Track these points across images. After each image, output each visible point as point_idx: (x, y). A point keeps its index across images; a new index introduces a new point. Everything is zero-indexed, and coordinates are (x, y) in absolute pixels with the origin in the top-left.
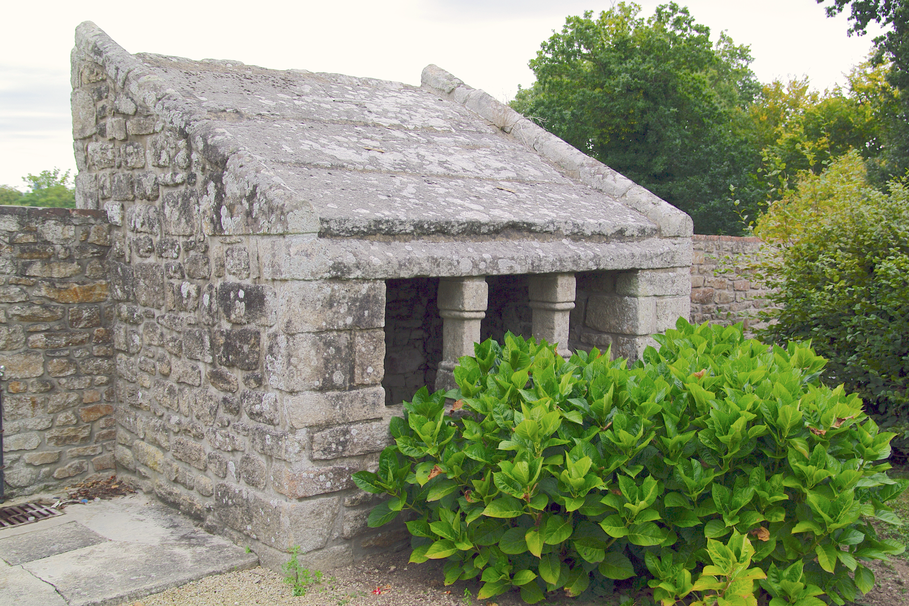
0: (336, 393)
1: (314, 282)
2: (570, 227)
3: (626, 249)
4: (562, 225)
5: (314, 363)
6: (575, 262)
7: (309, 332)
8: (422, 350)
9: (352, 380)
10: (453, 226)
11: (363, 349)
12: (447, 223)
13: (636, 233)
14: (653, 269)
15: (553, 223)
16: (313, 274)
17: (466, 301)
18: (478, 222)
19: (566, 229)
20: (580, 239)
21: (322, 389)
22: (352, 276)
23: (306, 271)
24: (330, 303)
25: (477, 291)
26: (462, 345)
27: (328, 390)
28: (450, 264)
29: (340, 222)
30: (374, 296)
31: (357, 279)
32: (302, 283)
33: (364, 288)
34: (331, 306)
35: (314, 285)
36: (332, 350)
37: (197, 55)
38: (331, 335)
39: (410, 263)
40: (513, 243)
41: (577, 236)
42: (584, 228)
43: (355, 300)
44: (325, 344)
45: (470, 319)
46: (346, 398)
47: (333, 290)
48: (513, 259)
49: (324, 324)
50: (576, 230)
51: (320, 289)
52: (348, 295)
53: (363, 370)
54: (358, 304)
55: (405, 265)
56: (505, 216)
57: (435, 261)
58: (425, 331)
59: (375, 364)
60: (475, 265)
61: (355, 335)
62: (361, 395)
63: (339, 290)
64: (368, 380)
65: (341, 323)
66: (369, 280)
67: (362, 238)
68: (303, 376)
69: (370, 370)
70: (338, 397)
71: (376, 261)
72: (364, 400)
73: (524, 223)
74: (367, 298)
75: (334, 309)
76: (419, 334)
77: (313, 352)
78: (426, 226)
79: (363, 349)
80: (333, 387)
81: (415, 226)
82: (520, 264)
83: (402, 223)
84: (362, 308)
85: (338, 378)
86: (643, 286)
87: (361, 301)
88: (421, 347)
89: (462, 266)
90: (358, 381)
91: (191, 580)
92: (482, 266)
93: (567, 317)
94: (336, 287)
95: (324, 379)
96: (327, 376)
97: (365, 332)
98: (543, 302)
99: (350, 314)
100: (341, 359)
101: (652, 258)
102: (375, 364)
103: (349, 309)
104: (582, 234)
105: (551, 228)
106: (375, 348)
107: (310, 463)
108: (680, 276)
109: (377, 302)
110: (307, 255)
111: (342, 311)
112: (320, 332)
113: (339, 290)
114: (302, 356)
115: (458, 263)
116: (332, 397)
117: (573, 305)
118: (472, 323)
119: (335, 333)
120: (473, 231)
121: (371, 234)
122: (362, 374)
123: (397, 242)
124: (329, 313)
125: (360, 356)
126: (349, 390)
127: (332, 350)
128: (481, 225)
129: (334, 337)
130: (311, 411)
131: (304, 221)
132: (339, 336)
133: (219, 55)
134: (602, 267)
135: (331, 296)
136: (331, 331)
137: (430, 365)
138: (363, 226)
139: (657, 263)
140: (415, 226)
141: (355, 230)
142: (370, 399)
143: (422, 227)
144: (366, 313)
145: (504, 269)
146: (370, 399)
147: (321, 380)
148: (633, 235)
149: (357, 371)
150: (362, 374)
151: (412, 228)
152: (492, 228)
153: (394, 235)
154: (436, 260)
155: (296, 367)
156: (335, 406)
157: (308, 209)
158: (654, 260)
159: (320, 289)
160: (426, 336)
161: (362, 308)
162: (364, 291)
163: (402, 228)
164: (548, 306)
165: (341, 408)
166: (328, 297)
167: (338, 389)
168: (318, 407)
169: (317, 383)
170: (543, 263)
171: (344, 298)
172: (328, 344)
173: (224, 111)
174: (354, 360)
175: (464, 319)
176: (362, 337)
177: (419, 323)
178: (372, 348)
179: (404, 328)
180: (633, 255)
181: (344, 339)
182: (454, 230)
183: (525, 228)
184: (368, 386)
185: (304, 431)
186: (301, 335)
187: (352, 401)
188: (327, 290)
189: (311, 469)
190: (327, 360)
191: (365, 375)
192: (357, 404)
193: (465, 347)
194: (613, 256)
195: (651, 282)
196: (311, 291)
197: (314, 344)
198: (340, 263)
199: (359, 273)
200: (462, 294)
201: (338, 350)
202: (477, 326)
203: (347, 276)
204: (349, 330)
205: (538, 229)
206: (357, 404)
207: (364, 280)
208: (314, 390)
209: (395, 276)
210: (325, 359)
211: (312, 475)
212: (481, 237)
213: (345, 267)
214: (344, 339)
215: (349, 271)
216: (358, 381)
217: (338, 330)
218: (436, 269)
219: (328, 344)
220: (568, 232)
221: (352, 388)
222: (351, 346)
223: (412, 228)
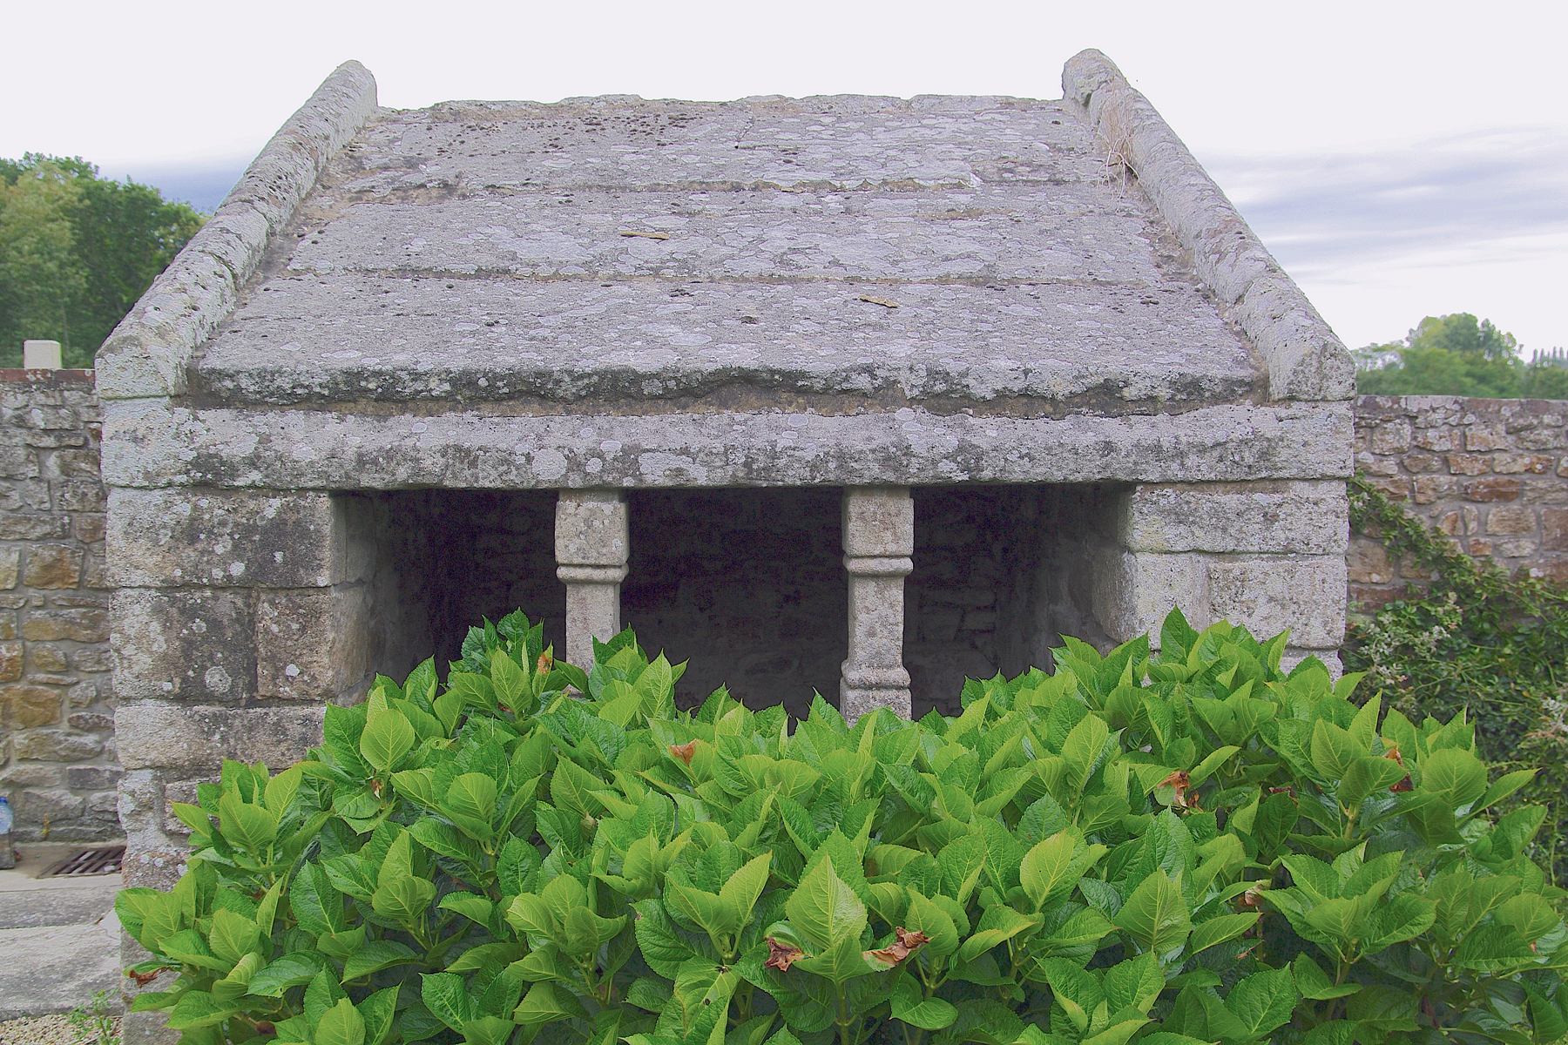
0: (216, 709)
1: (157, 492)
2: (920, 379)
3: (1127, 433)
4: (903, 376)
5: (160, 645)
6: (887, 460)
7: (148, 588)
9: (252, 686)
10: (558, 382)
11: (275, 628)
12: (539, 374)
13: (1164, 393)
14: (1190, 483)
15: (869, 370)
16: (147, 475)
18: (627, 370)
19: (911, 384)
20: (956, 410)
21: (182, 699)
22: (240, 482)
23: (134, 471)
24: (190, 532)
27: (198, 702)
28: (504, 461)
29: (262, 374)
30: (297, 523)
31: (253, 486)
32: (130, 493)
33: (272, 507)
34: (193, 540)
35: (157, 497)
36: (200, 625)
37: (550, 95)
38: (198, 594)
39: (389, 458)
40: (717, 419)
41: (946, 398)
42: (970, 381)
43: (248, 530)
44: (182, 611)
46: (237, 722)
47: (196, 508)
48: (685, 451)
49: (178, 573)
50: (940, 387)
51: (168, 505)
52: (231, 518)
53: (277, 670)
54: (257, 538)
55: (375, 462)
56: (743, 355)
57: (465, 455)
59: (305, 659)
60: (575, 463)
61: (258, 598)
62: (272, 719)
63: (211, 509)
64: (286, 691)
65: (218, 573)
66: (286, 491)
67: (322, 409)
68: (136, 669)
69: (292, 670)
70: (217, 719)
71: (304, 453)
72: (279, 729)
73: (773, 372)
74: (278, 525)
75: (199, 546)
77: (156, 626)
78: (483, 382)
79: (275, 628)
80: (209, 698)
81: (454, 382)
82: (704, 463)
83: (416, 376)
84: (268, 546)
85: (216, 679)
86: (1145, 526)
87: (265, 531)
89: (536, 467)
90: (263, 690)
91: (26, 1014)
92: (594, 466)
93: (897, 593)
94: (204, 503)
95: (185, 680)
96: (191, 673)
97: (282, 594)
99: (240, 558)
100: (225, 644)
101: (1181, 455)
102: (305, 659)
103: (236, 546)
104: (967, 397)
105: (863, 382)
106: (303, 629)
107: (163, 839)
108: (1299, 503)
110: (135, 440)
111: (219, 549)
112: (169, 587)
113: (211, 509)
114: (132, 632)
115: (529, 458)
116: (204, 717)
117: (908, 565)
119: (208, 593)
120: (618, 391)
121: (341, 400)
122: (274, 678)
123: (408, 416)
124: (190, 554)
125: (269, 642)
126: (248, 706)
127: (200, 625)
128: (637, 378)
129: (205, 600)
130: (156, 738)
131: (129, 375)
132: (216, 598)
133: (830, 88)
134: (987, 474)
135: (192, 520)
136: (202, 587)
138: (318, 382)
139: (1201, 467)
140: (454, 382)
141: (299, 391)
142: (295, 730)
143: (472, 384)
144: (279, 556)
145: (655, 473)
146: (295, 730)
147: (177, 680)
148: (1152, 399)
149: (263, 670)
150: (274, 678)
151: (447, 387)
152: (672, 384)
153: (404, 402)
154: (468, 452)
155: (118, 650)
156: (211, 733)
157: (137, 351)
158: (1192, 460)
159: (168, 505)
161: (268, 546)
162: (270, 513)
163: (420, 386)
165: (224, 739)
166: (185, 522)
167: (221, 701)
168: (170, 732)
169: (168, 686)
170: (782, 462)
171: (223, 524)
172: (190, 613)
173: (423, 186)
174: (256, 649)
176: (272, 603)
178: (295, 626)
180: (1108, 447)
181: (227, 605)
182: (568, 388)
183: (780, 385)
184: (291, 701)
185: (147, 775)
186: (129, 592)
187: (251, 730)
188: (184, 509)
189: (162, 849)
190: (189, 645)
191: (280, 681)
192: (262, 737)
194: (1019, 451)
195: (1179, 517)
196: (146, 507)
197: (157, 610)
198: (211, 456)
199: (255, 476)
201: (215, 624)
203: (228, 482)
204: (244, 587)
205: (818, 386)
206: (262, 737)
207: (276, 491)
208: (161, 697)
209: (348, 485)
210: (184, 640)
211: (160, 862)
212: (646, 405)
213: (223, 463)
214: (227, 605)
215: (233, 472)
216: (263, 690)
217: (214, 587)
218: (467, 473)
219: (190, 613)
220: (916, 392)
221: (252, 703)
222: (248, 622)
223: (447, 387)
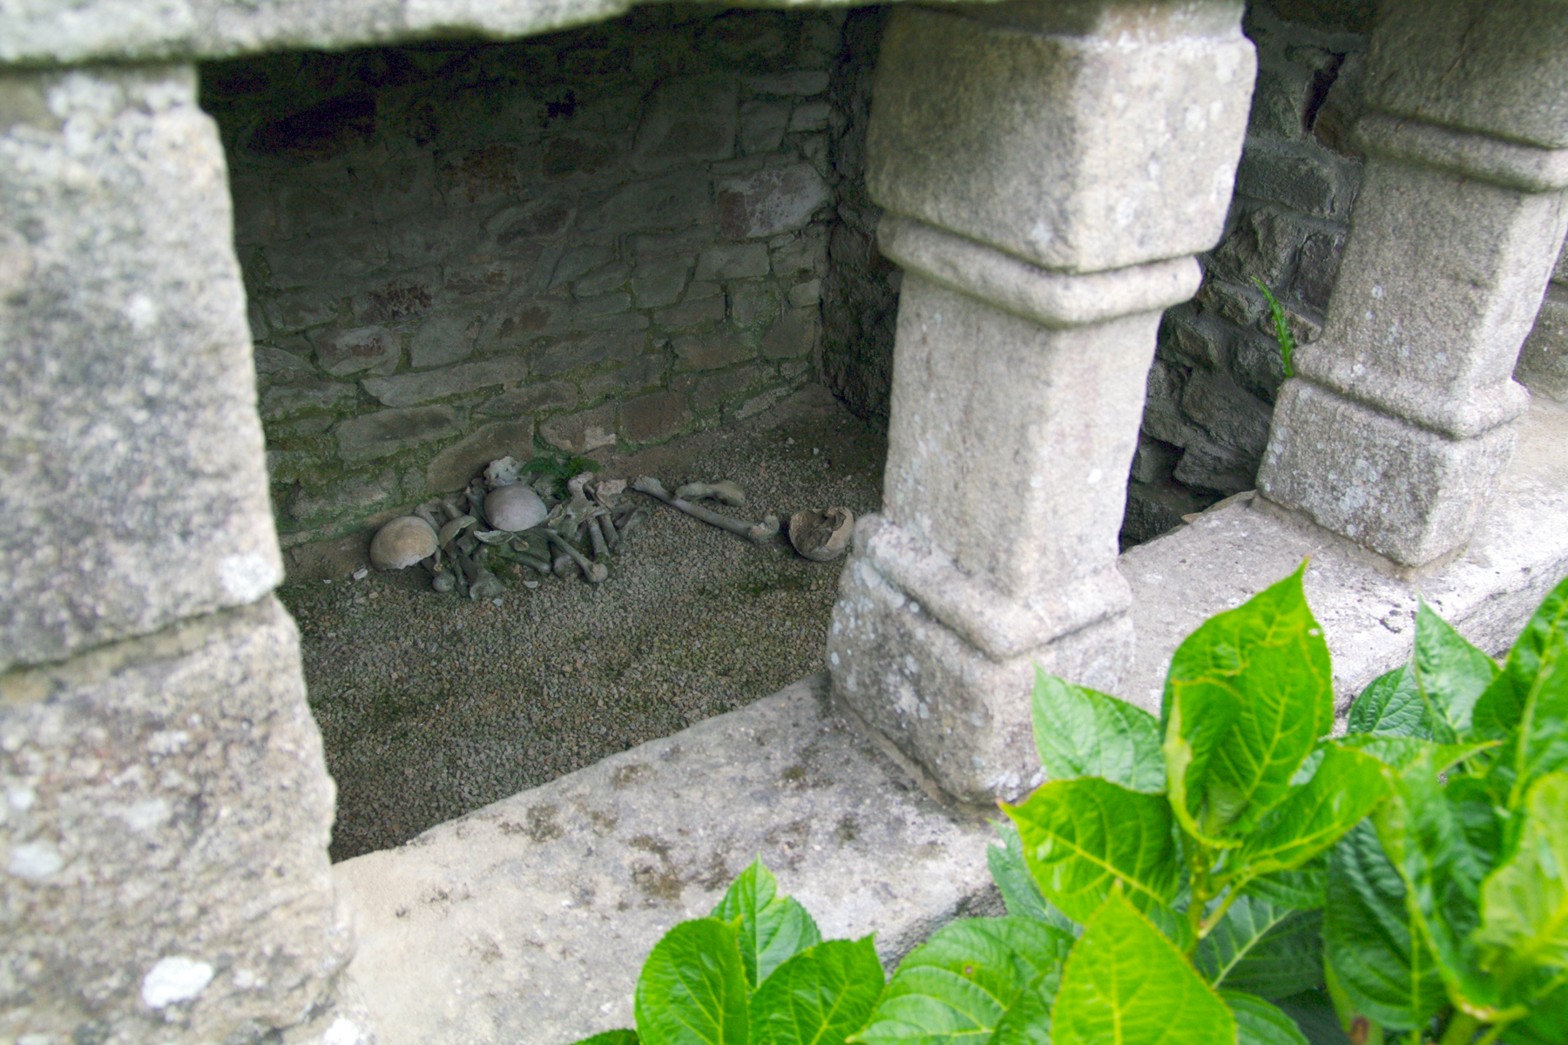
8: (824, 167)
17: (1092, 200)
25: (1175, 113)
26: (1021, 488)
45: (1101, 322)
58: (837, 107)
76: (815, 116)
88: (821, 156)
98: (1456, 129)
109: (101, 358)
118: (1100, 343)
137: (846, 214)
160: (838, 122)
164: (1482, 156)
175: (1047, 326)
177: (819, 82)
178: (148, 815)
179: (771, 98)
193: (1037, 506)
200: (1065, 136)
202: (1136, 352)
